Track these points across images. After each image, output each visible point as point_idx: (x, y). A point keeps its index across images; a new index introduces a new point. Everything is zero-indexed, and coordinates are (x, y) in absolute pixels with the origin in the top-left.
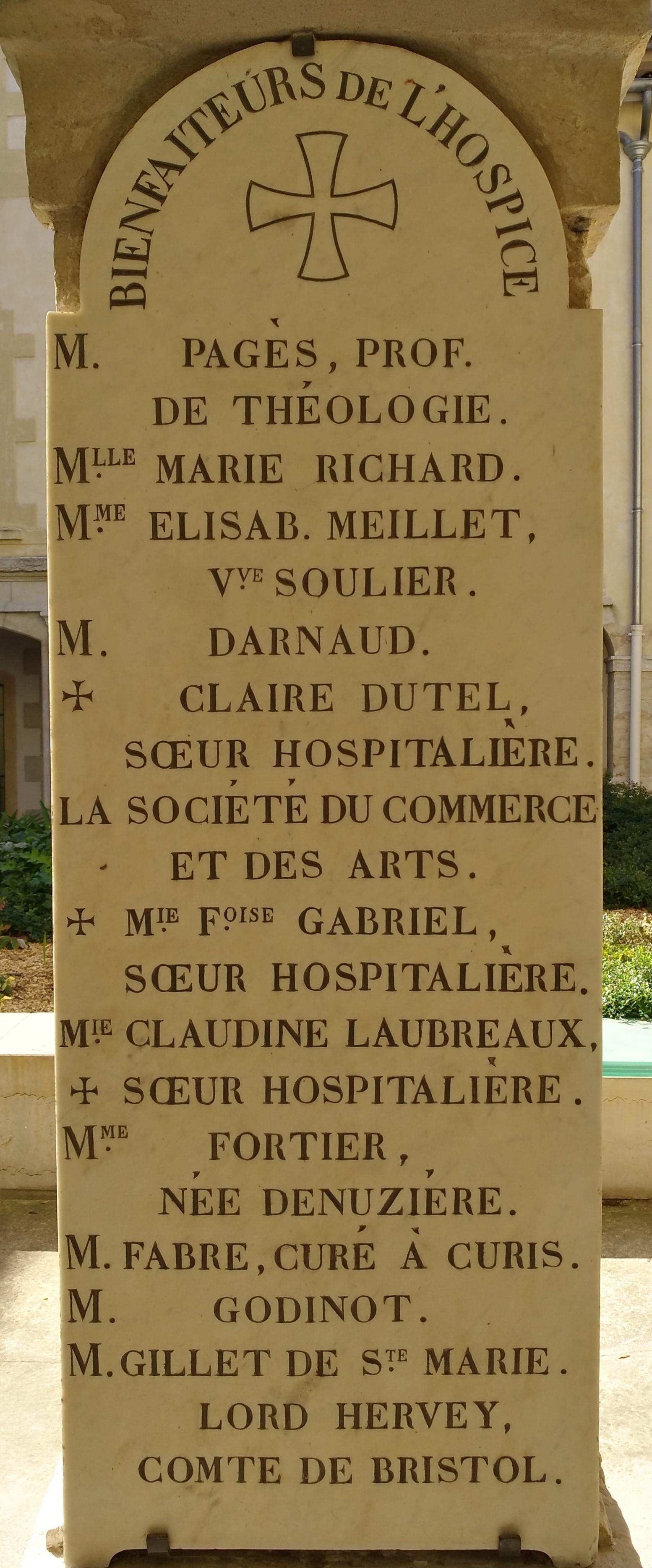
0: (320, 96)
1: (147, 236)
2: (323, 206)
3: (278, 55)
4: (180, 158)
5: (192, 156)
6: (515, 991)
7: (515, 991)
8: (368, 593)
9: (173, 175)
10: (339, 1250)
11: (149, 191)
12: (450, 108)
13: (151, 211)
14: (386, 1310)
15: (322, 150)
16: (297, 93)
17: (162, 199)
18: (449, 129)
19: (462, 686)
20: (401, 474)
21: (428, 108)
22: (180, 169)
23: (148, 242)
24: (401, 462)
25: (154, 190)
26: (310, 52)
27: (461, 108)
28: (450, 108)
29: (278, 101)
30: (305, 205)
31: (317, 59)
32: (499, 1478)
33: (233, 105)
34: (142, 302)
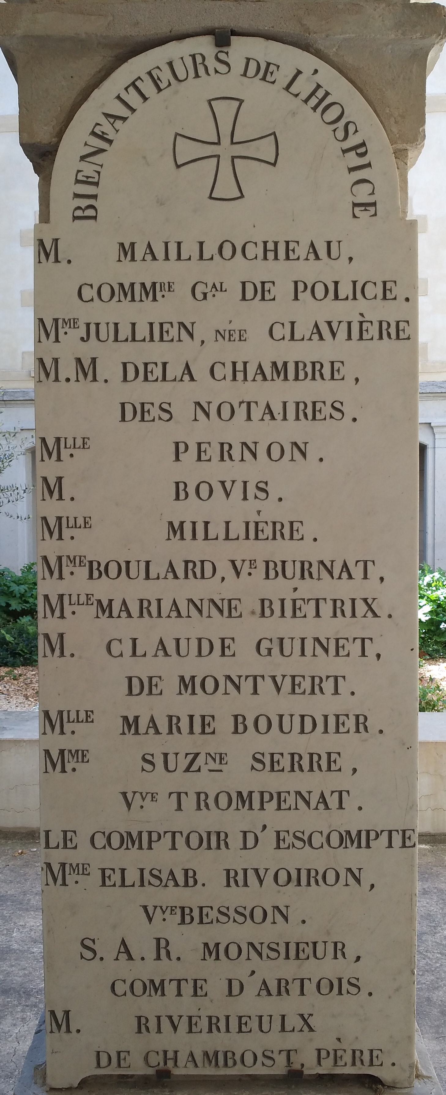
0: (229, 71)
1: (98, 168)
2: (226, 150)
3: (204, 46)
4: (123, 112)
5: (133, 110)
6: (270, 300)
7: (270, 300)
8: (116, 340)
9: (118, 124)
10: (226, 447)
11: (102, 137)
12: (319, 86)
13: (103, 151)
14: (241, 412)
15: (225, 111)
16: (211, 71)
17: (110, 142)
18: (320, 100)
19: (150, 73)
20: (240, 376)
21: (303, 86)
22: (124, 119)
23: (99, 173)
24: (240, 367)
25: (105, 136)
26: (228, 44)
27: (326, 86)
28: (319, 86)
29: (197, 76)
30: (226, 140)
31: (231, 50)
32: (189, 846)
33: (166, 75)
34: (95, 218)
